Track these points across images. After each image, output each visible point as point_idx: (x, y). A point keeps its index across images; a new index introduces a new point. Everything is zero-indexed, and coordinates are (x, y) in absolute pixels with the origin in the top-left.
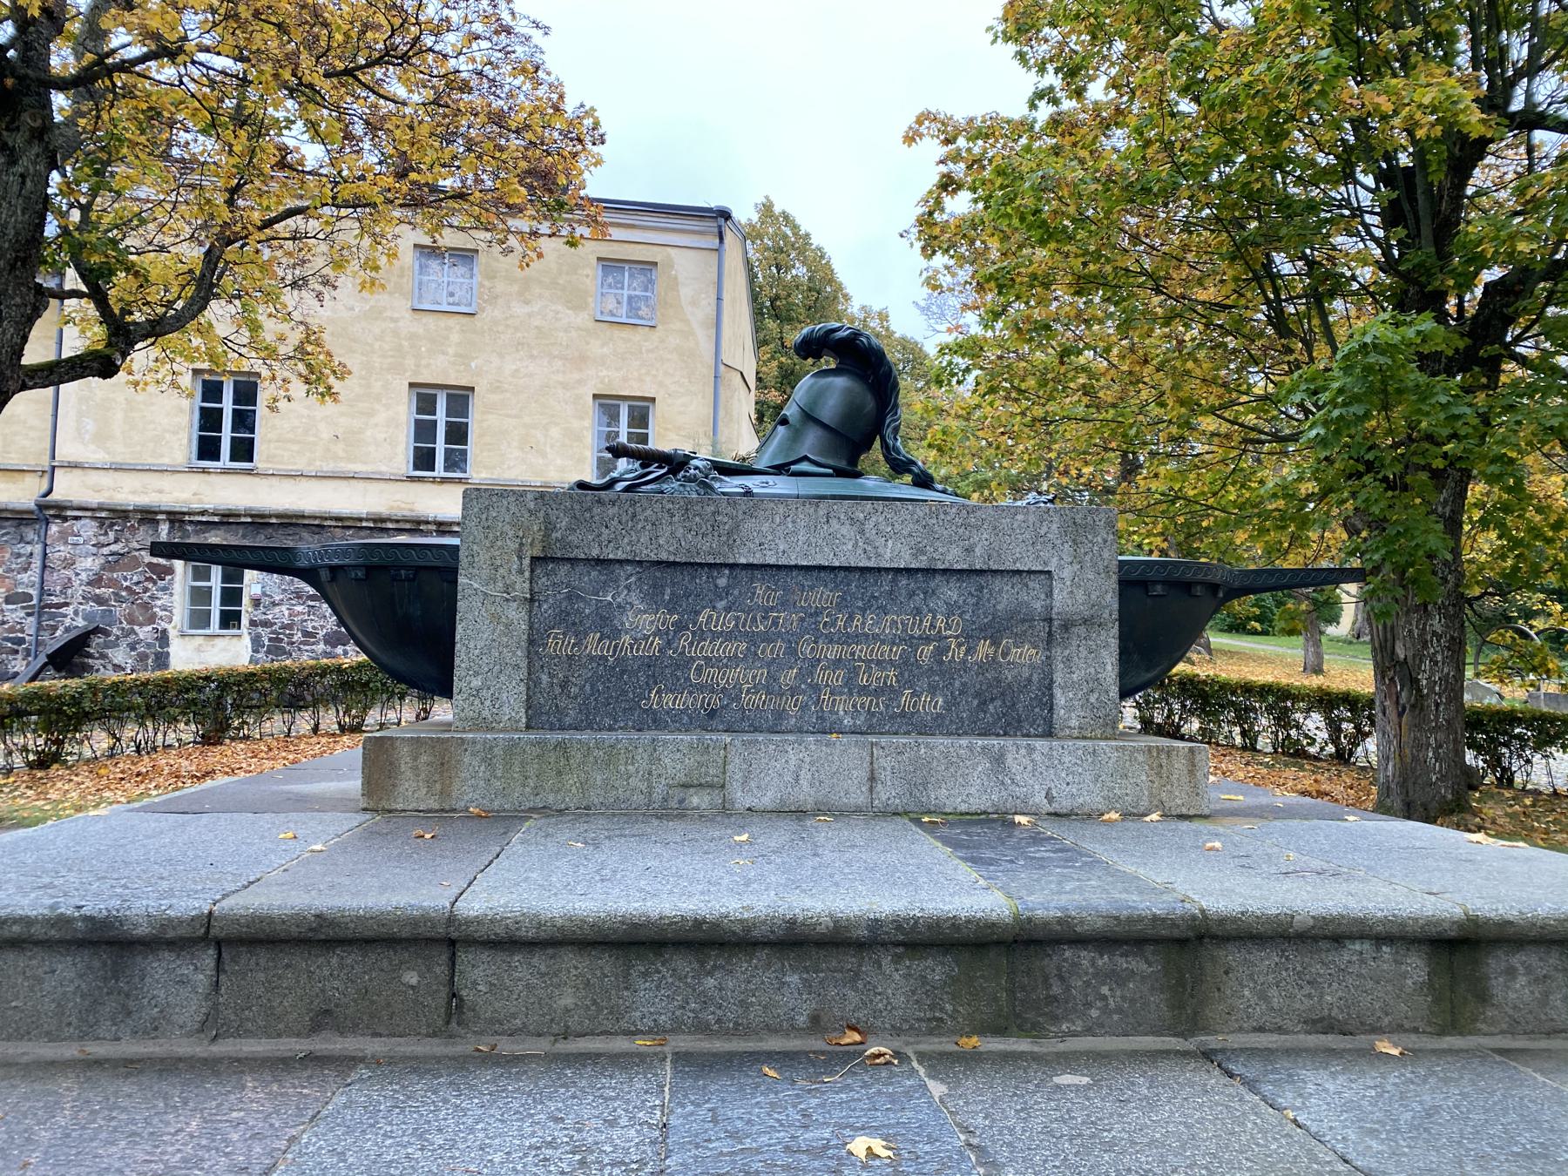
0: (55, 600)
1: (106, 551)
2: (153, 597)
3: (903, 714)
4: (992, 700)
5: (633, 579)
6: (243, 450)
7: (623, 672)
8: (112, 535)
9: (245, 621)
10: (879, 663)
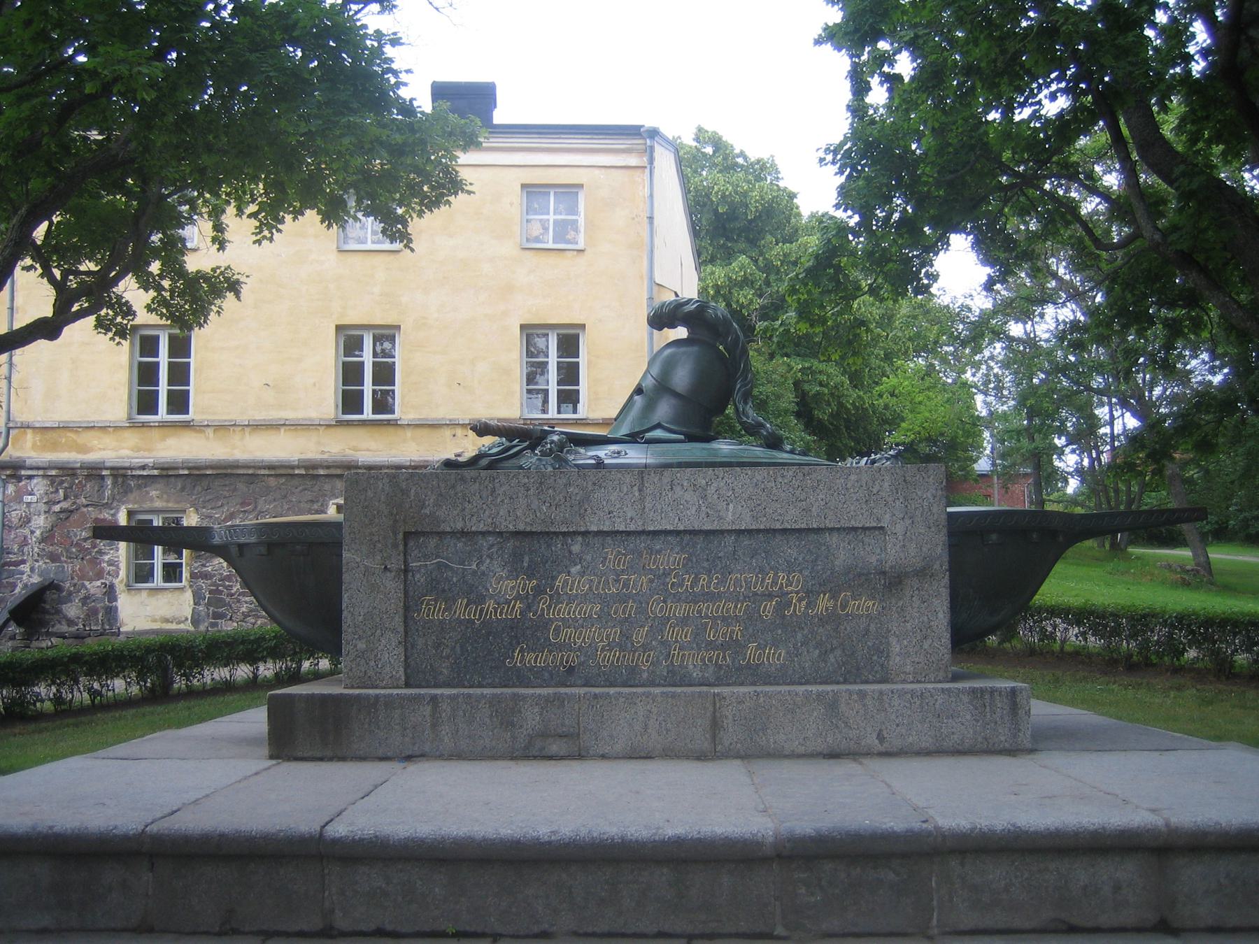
0: (13, 558)
1: (57, 508)
2: (101, 553)
3: (748, 666)
4: (832, 650)
5: (494, 549)
6: (179, 402)
7: (489, 634)
8: (61, 492)
9: (186, 574)
10: (724, 619)
